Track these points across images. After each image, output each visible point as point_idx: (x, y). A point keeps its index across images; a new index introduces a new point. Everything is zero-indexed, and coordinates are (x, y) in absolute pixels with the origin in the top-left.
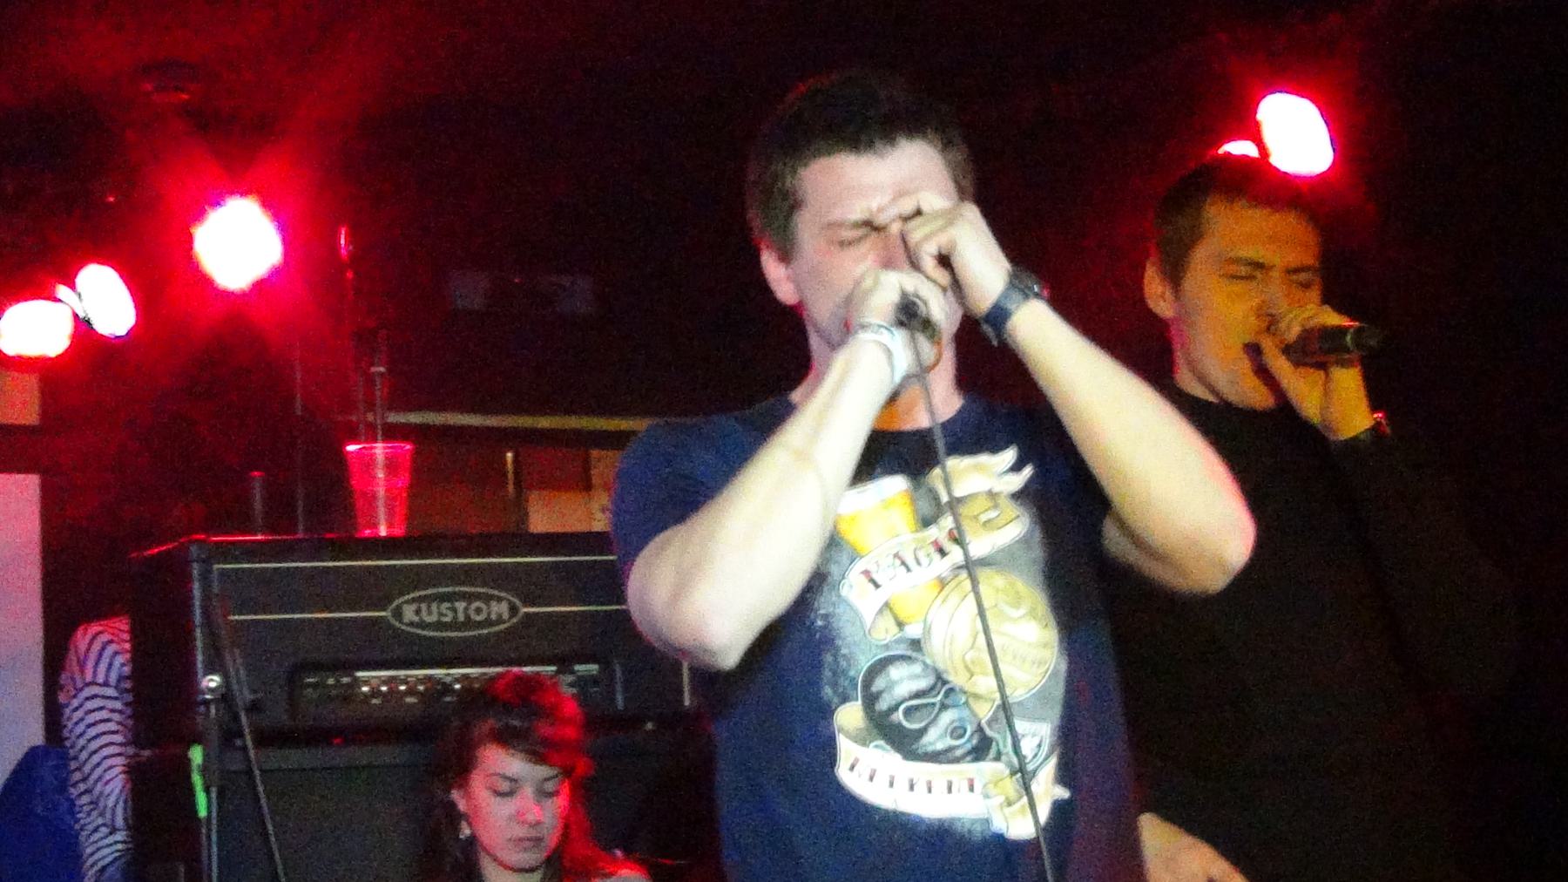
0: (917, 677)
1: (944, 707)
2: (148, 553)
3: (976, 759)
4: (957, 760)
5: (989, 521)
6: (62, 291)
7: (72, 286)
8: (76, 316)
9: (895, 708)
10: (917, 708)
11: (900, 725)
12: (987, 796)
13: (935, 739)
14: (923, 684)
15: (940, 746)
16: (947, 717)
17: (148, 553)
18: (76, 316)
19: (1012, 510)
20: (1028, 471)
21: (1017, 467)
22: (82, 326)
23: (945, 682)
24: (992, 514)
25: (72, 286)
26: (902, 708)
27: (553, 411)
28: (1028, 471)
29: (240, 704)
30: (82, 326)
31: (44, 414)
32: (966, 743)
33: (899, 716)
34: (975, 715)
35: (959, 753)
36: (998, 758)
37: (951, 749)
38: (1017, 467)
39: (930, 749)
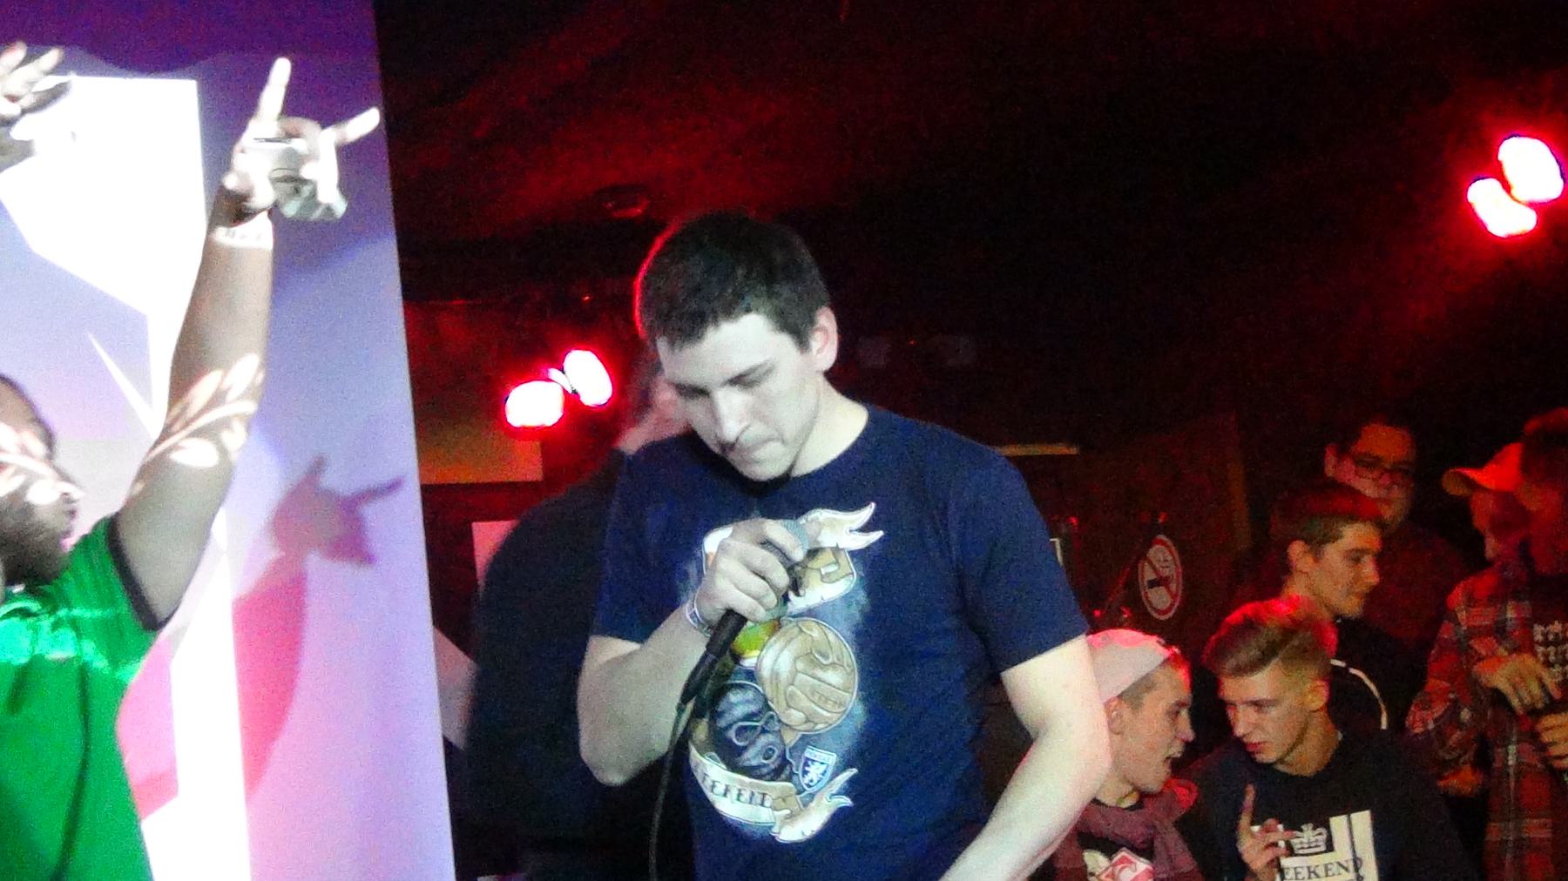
0: (748, 701)
1: (764, 731)
2: (1376, 693)
3: (772, 780)
4: (760, 777)
5: (828, 574)
6: (554, 373)
7: (562, 370)
8: (565, 392)
9: (730, 726)
10: (745, 728)
11: (731, 741)
12: (775, 809)
13: (752, 757)
14: (753, 708)
15: (754, 763)
16: (764, 740)
17: (1376, 693)
18: (565, 392)
19: (847, 564)
20: (877, 535)
21: (867, 528)
22: (571, 400)
23: (770, 709)
24: (833, 568)
25: (562, 370)
26: (735, 727)
27: (1052, 458)
28: (877, 535)
29: (85, 572)
30: (571, 400)
31: (546, 470)
32: (773, 763)
33: (732, 734)
34: (782, 741)
35: (765, 770)
36: (789, 779)
37: (759, 767)
38: (867, 528)
39: (747, 764)
